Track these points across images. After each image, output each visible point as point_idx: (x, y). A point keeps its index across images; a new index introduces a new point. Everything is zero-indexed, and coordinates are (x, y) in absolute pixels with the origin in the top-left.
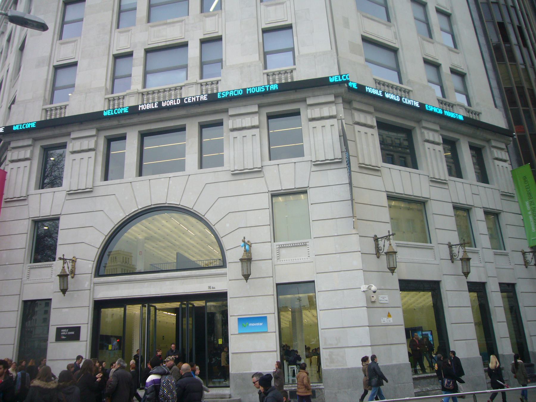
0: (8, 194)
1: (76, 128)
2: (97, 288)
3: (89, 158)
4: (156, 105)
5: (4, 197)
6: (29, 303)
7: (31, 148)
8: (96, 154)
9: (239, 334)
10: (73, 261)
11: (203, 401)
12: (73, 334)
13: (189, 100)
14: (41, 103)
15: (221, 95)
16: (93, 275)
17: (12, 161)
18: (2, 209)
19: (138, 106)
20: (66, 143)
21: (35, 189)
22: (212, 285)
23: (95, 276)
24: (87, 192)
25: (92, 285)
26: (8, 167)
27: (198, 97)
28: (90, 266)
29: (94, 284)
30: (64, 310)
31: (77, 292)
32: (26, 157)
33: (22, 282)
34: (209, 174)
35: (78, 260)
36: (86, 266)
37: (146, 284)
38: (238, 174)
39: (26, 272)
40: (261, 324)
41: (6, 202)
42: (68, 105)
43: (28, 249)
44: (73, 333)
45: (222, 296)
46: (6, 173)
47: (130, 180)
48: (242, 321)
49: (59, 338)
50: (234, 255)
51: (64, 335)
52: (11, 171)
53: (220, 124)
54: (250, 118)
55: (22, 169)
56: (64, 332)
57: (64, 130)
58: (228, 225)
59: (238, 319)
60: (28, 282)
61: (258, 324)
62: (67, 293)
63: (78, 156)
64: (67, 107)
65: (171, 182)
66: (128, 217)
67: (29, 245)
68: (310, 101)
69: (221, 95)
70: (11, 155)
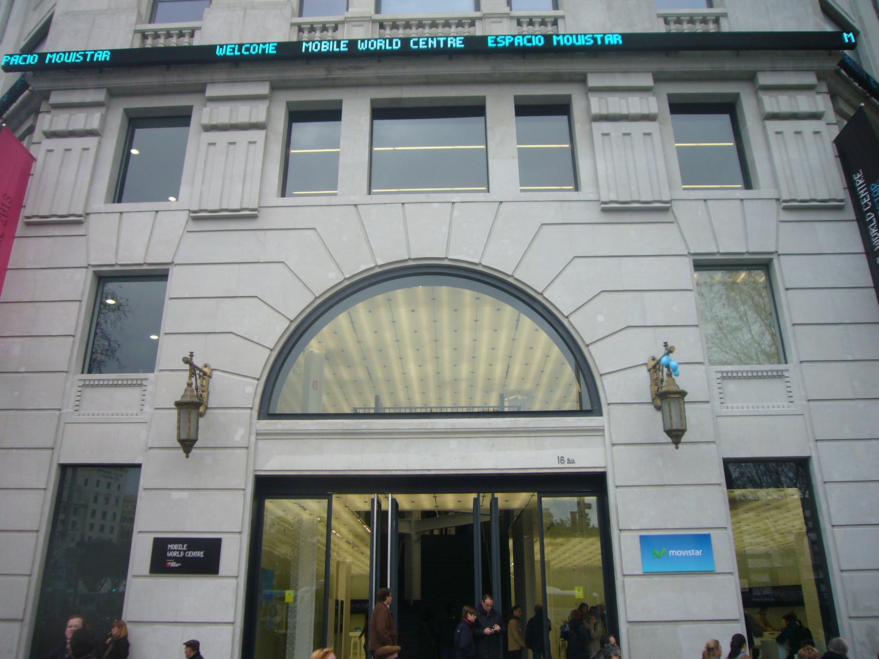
0: (36, 202)
1: (221, 76)
2: (264, 445)
3: (84, 149)
4: (342, 45)
5: (25, 212)
6: (69, 471)
7: (103, 110)
8: (100, 143)
9: (646, 574)
10: (205, 374)
11: (852, 632)
12: (202, 557)
13: (421, 43)
14: (134, 19)
15: (496, 42)
16: (255, 414)
17: (52, 135)
18: (16, 242)
19: (300, 43)
20: (190, 108)
21: (106, 202)
22: (567, 454)
23: (260, 417)
24: (244, 216)
25: (253, 438)
26: (41, 149)
27: (442, 39)
28: (250, 390)
29: (257, 434)
30: (176, 495)
31: (211, 451)
32: (88, 128)
33: (60, 417)
34: (550, 204)
35: (214, 373)
36: (236, 390)
37: (397, 443)
38: (617, 210)
39: (73, 393)
40: (699, 553)
41: (28, 224)
42: (199, 28)
43: (81, 340)
44: (200, 554)
45: (594, 483)
46: (33, 159)
47: (354, 199)
48: (649, 543)
49: (161, 563)
50: (624, 384)
51: (176, 559)
52: (46, 157)
53: (182, 118)
54: (85, 114)
55: (75, 154)
56: (174, 550)
57: (190, 78)
58: (600, 318)
59: (641, 537)
60: (75, 417)
61: (691, 553)
62: (193, 451)
63: (59, 144)
64: (197, 33)
65: (456, 213)
66: (347, 283)
67: (83, 331)
68: (211, 92)
69: (496, 42)
70: (45, 122)
